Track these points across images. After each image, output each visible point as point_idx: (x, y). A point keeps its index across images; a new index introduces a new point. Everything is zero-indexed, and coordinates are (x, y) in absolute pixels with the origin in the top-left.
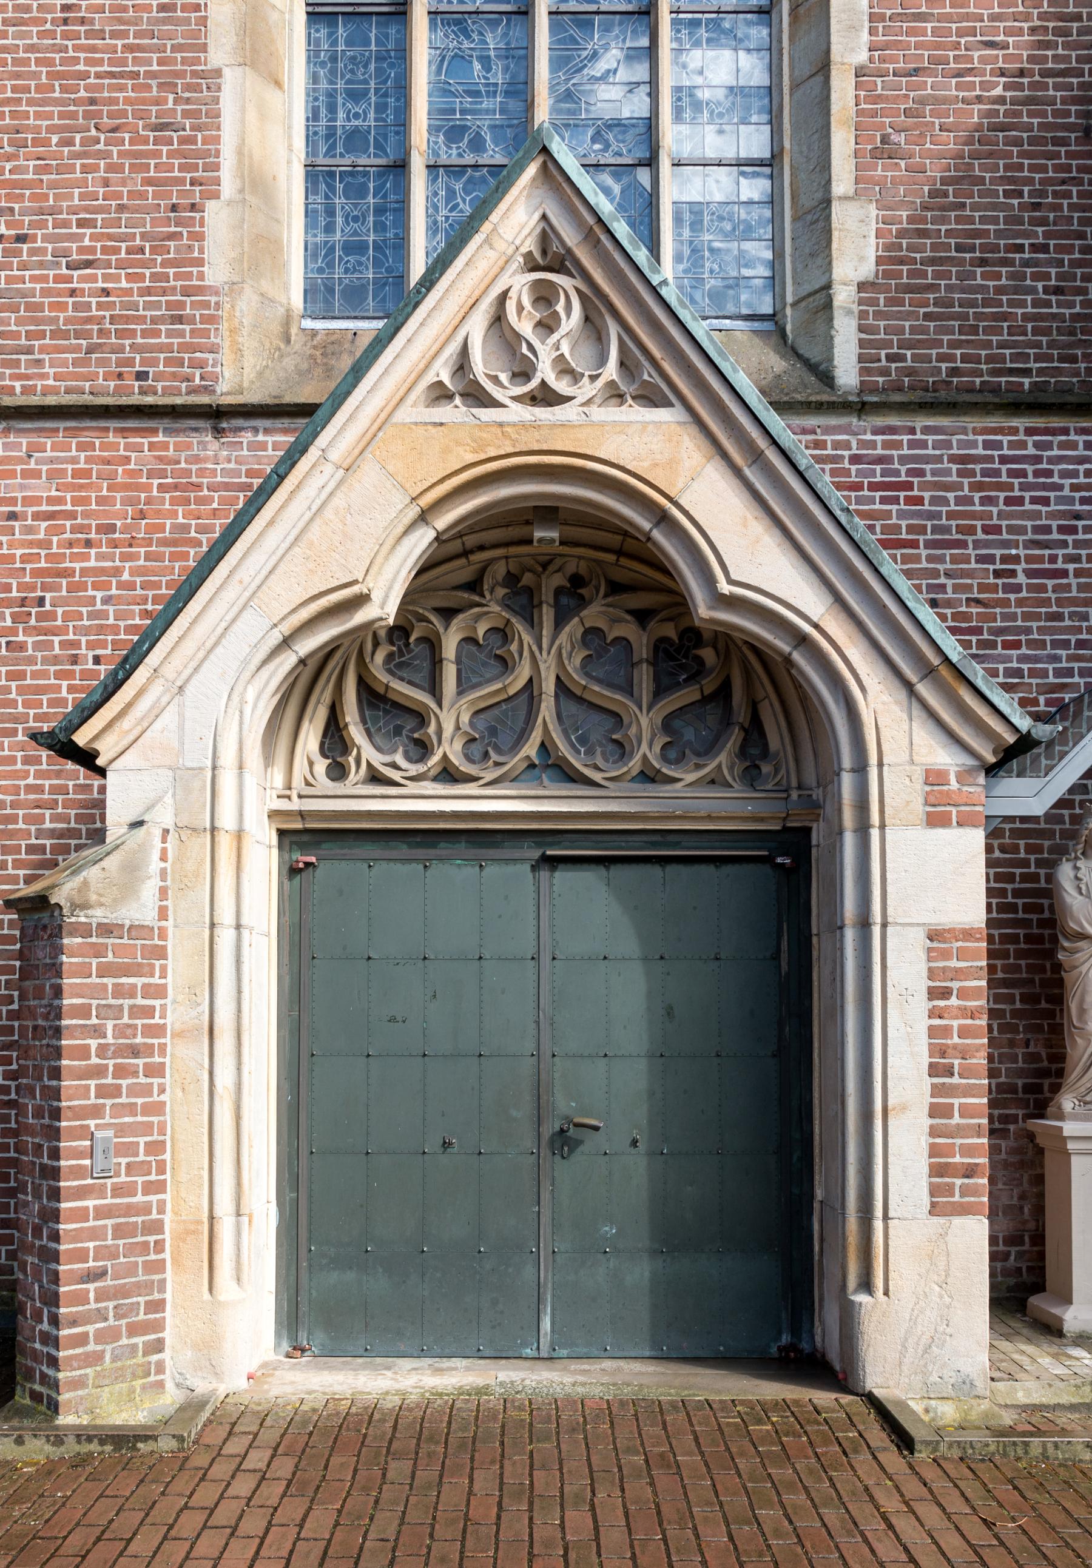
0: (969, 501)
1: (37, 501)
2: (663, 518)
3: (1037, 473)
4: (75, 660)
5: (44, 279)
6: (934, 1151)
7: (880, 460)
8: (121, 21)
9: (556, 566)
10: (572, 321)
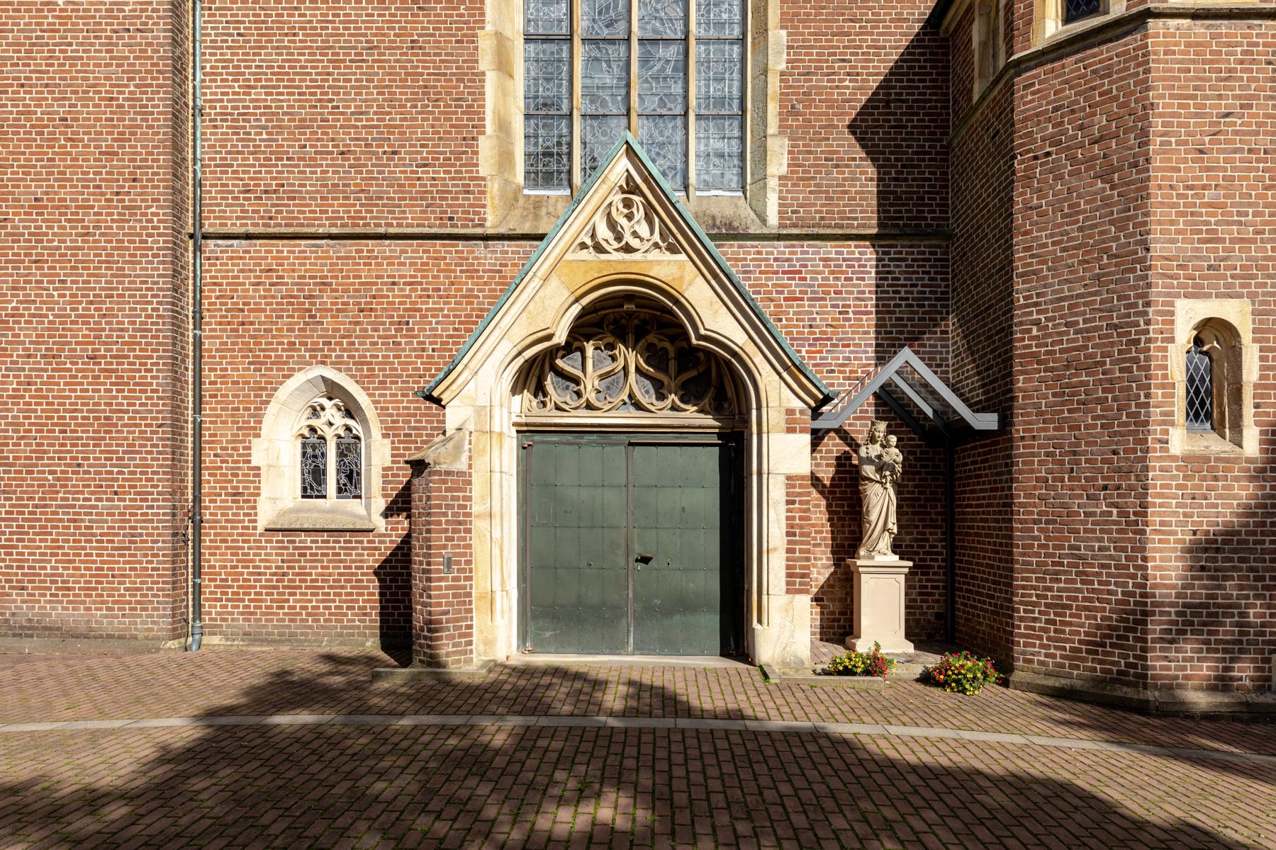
0: (827, 279)
1: (405, 276)
2: (677, 302)
3: (860, 266)
4: (423, 350)
5: (405, 172)
6: (788, 567)
7: (788, 260)
8: (438, 48)
9: (629, 318)
10: (639, 214)
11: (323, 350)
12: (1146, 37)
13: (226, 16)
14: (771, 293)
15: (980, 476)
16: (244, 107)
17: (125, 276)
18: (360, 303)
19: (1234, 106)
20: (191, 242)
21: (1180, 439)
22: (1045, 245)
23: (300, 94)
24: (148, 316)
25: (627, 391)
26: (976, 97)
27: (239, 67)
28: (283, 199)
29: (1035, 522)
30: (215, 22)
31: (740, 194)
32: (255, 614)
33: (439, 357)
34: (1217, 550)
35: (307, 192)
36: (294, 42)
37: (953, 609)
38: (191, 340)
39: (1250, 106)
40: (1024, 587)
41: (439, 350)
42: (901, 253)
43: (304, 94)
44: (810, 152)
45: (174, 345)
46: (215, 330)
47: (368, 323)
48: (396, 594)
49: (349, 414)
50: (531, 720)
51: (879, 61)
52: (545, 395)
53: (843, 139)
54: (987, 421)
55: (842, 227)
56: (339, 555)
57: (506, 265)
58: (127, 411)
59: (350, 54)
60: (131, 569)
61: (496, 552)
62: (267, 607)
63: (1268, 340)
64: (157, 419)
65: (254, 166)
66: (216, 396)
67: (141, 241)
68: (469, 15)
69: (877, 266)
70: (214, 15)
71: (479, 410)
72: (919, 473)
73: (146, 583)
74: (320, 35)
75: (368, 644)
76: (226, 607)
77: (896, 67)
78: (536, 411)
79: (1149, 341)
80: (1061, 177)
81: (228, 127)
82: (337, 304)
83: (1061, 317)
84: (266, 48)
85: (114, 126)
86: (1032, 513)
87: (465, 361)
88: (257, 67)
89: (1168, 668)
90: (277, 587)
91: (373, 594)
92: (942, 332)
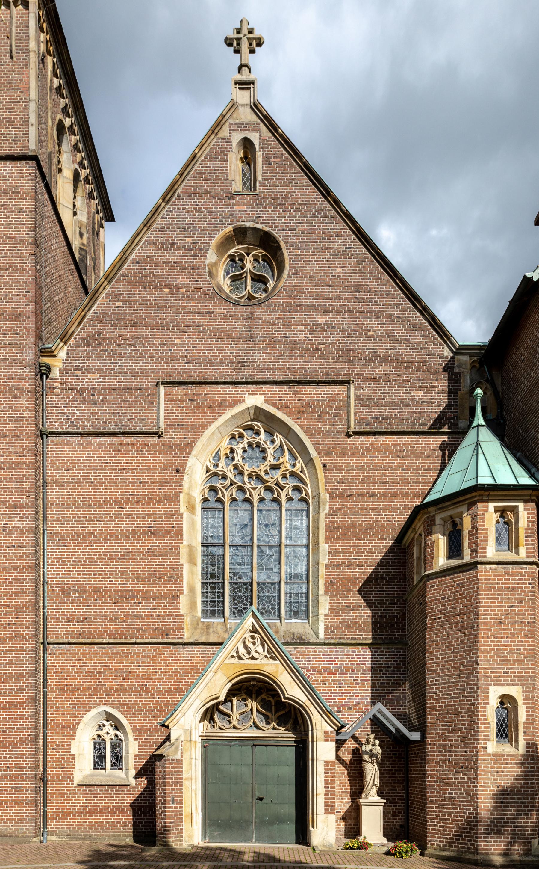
0: (348, 664)
1: (144, 663)
2: (275, 682)
4: (154, 698)
6: (325, 802)
7: (329, 655)
9: (253, 688)
10: (258, 643)
11: (105, 698)
12: (477, 572)
13: (58, 537)
14: (321, 670)
15: (416, 760)
16: (67, 581)
17: (12, 664)
18: (123, 676)
19: (515, 603)
20: (42, 646)
21: (492, 746)
22: (439, 659)
23: (94, 575)
24: (24, 683)
25: (252, 720)
26: (415, 583)
27: (65, 561)
28: (86, 625)
29: (435, 782)
30: (53, 540)
31: (306, 621)
32: (72, 825)
33: (161, 701)
34: (508, 795)
35: (98, 622)
36: (91, 549)
37: (408, 823)
38: (42, 693)
39: (522, 603)
40: (431, 811)
41: (162, 698)
42: (383, 652)
43: (96, 574)
44: (339, 603)
45: (36, 696)
46: (53, 688)
47: (127, 685)
48: (141, 816)
49: (116, 728)
50: (216, 863)
51: (373, 559)
52: (214, 722)
53: (355, 597)
54: (415, 736)
55: (354, 639)
56: (113, 797)
57: (193, 657)
58: (14, 728)
59: (118, 555)
60: (16, 804)
61: (193, 795)
62: (78, 822)
63: (529, 704)
64: (28, 732)
65: (72, 609)
66: (54, 720)
67: (20, 647)
68: (176, 537)
69: (372, 658)
70: (53, 536)
71: (186, 731)
72: (392, 757)
73: (23, 810)
74: (104, 546)
75: (128, 840)
76: (58, 822)
77: (381, 562)
78: (210, 729)
79: (478, 704)
80: (444, 629)
81: (59, 590)
82: (112, 676)
83: (445, 691)
84: (78, 552)
85: (7, 592)
86: (434, 778)
87: (180, 709)
88: (73, 561)
89: (487, 846)
90: (83, 813)
91: (129, 816)
92: (403, 690)
